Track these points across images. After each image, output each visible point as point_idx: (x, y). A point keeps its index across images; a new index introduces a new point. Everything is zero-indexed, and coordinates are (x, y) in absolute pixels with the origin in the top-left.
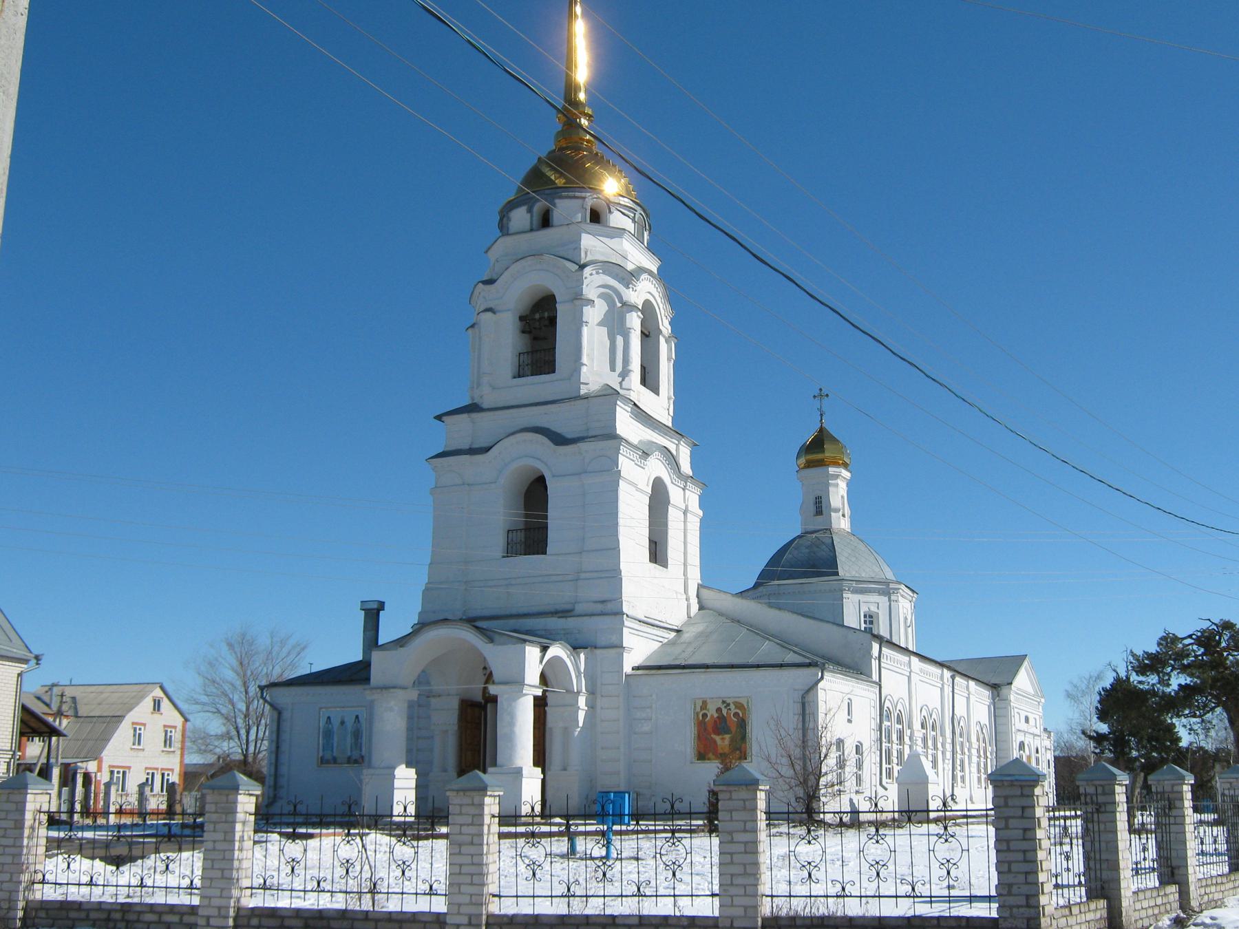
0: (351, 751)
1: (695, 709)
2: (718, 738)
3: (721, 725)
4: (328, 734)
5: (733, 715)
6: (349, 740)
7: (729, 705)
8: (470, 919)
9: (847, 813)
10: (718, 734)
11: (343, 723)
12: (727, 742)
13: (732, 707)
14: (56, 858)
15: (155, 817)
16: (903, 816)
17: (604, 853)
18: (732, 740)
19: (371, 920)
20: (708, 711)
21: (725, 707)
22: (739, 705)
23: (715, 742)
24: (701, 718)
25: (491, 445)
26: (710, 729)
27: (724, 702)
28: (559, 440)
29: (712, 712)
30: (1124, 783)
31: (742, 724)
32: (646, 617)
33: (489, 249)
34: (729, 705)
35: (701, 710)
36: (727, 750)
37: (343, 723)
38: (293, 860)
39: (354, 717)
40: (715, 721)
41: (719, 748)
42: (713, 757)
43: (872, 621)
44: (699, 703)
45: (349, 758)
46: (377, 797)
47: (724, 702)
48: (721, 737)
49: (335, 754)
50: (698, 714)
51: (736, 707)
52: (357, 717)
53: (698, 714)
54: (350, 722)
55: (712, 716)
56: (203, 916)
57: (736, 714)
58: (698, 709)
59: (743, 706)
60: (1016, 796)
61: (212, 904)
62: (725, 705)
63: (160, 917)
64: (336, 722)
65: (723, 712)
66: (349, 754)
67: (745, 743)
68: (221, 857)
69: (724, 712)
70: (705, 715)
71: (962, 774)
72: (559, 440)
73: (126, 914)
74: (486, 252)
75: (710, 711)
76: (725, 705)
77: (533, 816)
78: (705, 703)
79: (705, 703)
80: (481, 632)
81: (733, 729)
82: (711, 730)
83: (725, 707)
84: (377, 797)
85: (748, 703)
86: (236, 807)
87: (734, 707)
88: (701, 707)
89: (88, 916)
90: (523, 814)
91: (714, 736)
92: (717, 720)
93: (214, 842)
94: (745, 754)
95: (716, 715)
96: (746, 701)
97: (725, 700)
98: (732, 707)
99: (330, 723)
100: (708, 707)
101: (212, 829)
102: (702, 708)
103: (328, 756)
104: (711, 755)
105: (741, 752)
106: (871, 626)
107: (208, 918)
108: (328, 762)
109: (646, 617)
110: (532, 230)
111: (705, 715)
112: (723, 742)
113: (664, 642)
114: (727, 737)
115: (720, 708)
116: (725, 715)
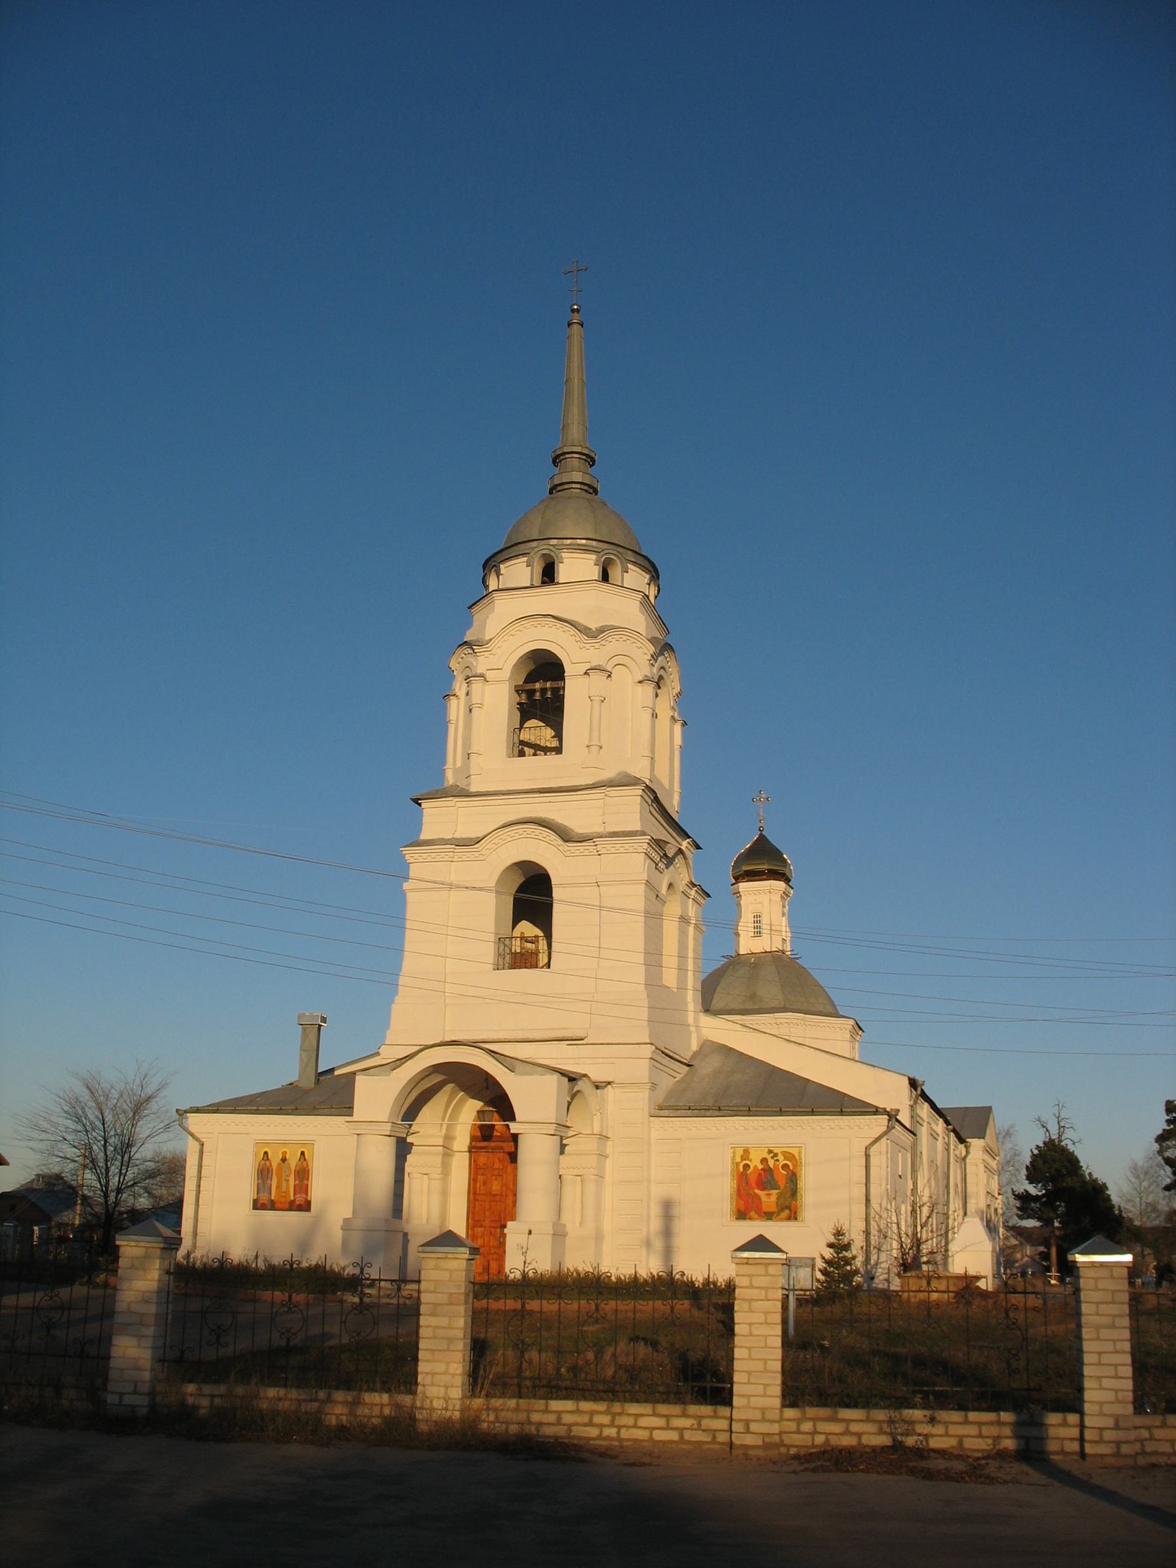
1: (733, 1159)
2: (761, 1194)
3: (766, 1178)
5: (782, 1168)
7: (776, 1155)
10: (763, 1189)
11: (284, 1160)
12: (773, 1198)
13: (780, 1157)
16: (935, 1287)
18: (779, 1197)
20: (751, 1161)
21: (772, 1158)
22: (789, 1156)
23: (758, 1198)
24: (741, 1170)
26: (753, 1180)
27: (770, 1152)
28: (565, 835)
29: (755, 1163)
31: (793, 1178)
35: (742, 1160)
36: (773, 1209)
38: (219, 1328)
39: (299, 1153)
40: (760, 1174)
41: (763, 1204)
42: (756, 1216)
44: (740, 1152)
46: (709, 1265)
47: (770, 1152)
48: (766, 1192)
49: (273, 1198)
50: (738, 1164)
51: (786, 1158)
52: (303, 1153)
53: (738, 1164)
54: (293, 1161)
55: (756, 1167)
56: (740, 1420)
57: (785, 1167)
58: (738, 1159)
59: (794, 1156)
61: (752, 1404)
63: (668, 1422)
64: (275, 1161)
65: (769, 1163)
66: (292, 1198)
67: (796, 1200)
68: (763, 1344)
69: (771, 1163)
70: (747, 1166)
72: (565, 835)
73: (617, 1417)
74: (470, 607)
75: (753, 1160)
77: (929, 1292)
78: (746, 1152)
79: (746, 1152)
81: (782, 1183)
82: (754, 1185)
83: (772, 1158)
84: (709, 1265)
85: (800, 1153)
87: (783, 1157)
88: (742, 1157)
89: (559, 1419)
91: (757, 1191)
92: (762, 1172)
93: (750, 1324)
94: (795, 1213)
95: (760, 1167)
96: (798, 1152)
98: (780, 1157)
99: (268, 1159)
100: (750, 1157)
102: (743, 1158)
103: (264, 1198)
104: (753, 1214)
105: (791, 1211)
107: (747, 1423)
109: (666, 1048)
110: (532, 587)
111: (747, 1166)
112: (769, 1198)
114: (774, 1192)
115: (765, 1158)
116: (772, 1166)
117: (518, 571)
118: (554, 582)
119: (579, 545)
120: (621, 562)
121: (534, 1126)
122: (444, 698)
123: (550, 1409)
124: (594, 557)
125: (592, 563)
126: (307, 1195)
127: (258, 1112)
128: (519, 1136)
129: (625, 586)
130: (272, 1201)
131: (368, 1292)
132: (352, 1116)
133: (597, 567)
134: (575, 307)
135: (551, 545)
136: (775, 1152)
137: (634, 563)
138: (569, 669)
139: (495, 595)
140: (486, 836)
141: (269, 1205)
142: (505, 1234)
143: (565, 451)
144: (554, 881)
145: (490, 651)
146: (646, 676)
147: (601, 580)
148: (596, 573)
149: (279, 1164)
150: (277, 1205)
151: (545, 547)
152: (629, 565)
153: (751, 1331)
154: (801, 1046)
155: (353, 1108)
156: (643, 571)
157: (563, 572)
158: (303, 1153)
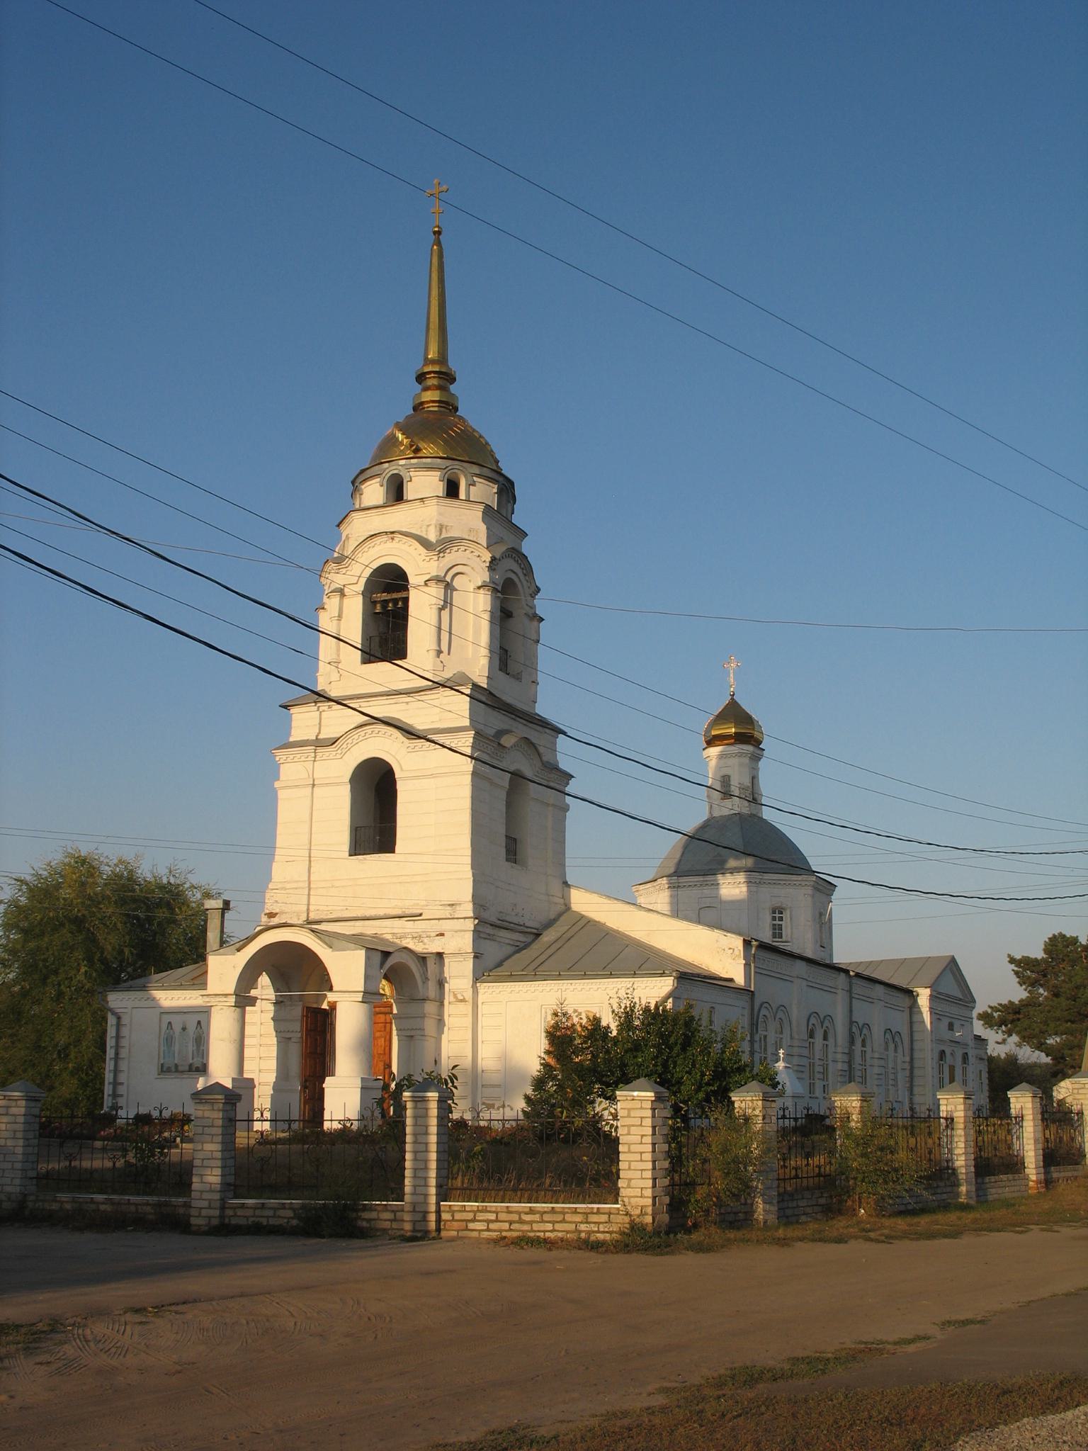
0: (193, 1059)
4: (169, 1040)
6: (191, 1047)
7: (580, 1014)
8: (210, 1204)
9: (257, 1120)
11: (184, 1029)
14: (443, 599)
15: (488, 1209)
17: (810, 1197)
19: (132, 1204)
21: (577, 1016)
25: (338, 736)
28: (410, 733)
30: (1038, 1096)
32: (499, 920)
33: (341, 523)
34: (580, 1014)
37: (184, 1029)
43: (782, 917)
45: (191, 1065)
49: (176, 1062)
52: (199, 1022)
60: (637, 1109)
62: (576, 1014)
64: (177, 1028)
66: (191, 1062)
71: (822, 1083)
72: (410, 733)
76: (576, 1014)
80: (320, 939)
83: (577, 1016)
86: (438, 1122)
90: (255, 1119)
97: (576, 1008)
101: (17, 1133)
106: (780, 923)
108: (169, 1070)
109: (499, 920)
113: (521, 946)
117: (374, 492)
118: (402, 499)
119: (424, 463)
120: (465, 476)
121: (347, 995)
122: (331, 618)
123: (469, 1228)
124: (438, 473)
125: (438, 478)
126: (203, 1058)
127: (163, 988)
128: (338, 1003)
129: (471, 499)
130: (176, 1066)
131: (284, 1135)
132: (206, 989)
133: (442, 483)
134: (436, 229)
135: (401, 465)
136: (580, 1011)
137: (479, 476)
138: (413, 580)
139: (353, 515)
140: (341, 737)
141: (173, 1069)
142: (324, 1089)
143: (425, 371)
144: (398, 774)
145: (346, 567)
146: (484, 581)
147: (445, 496)
148: (440, 488)
149: (180, 1033)
150: (180, 1068)
151: (394, 468)
152: (474, 478)
153: (201, 1194)
154: (399, 912)
155: (206, 984)
156: (490, 482)
157: (410, 491)
158: (199, 1022)
